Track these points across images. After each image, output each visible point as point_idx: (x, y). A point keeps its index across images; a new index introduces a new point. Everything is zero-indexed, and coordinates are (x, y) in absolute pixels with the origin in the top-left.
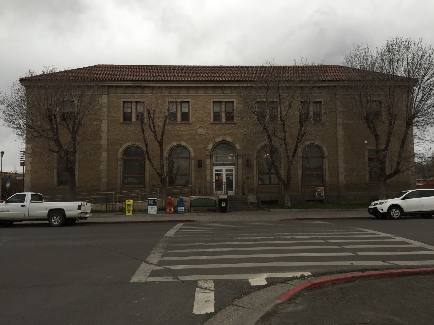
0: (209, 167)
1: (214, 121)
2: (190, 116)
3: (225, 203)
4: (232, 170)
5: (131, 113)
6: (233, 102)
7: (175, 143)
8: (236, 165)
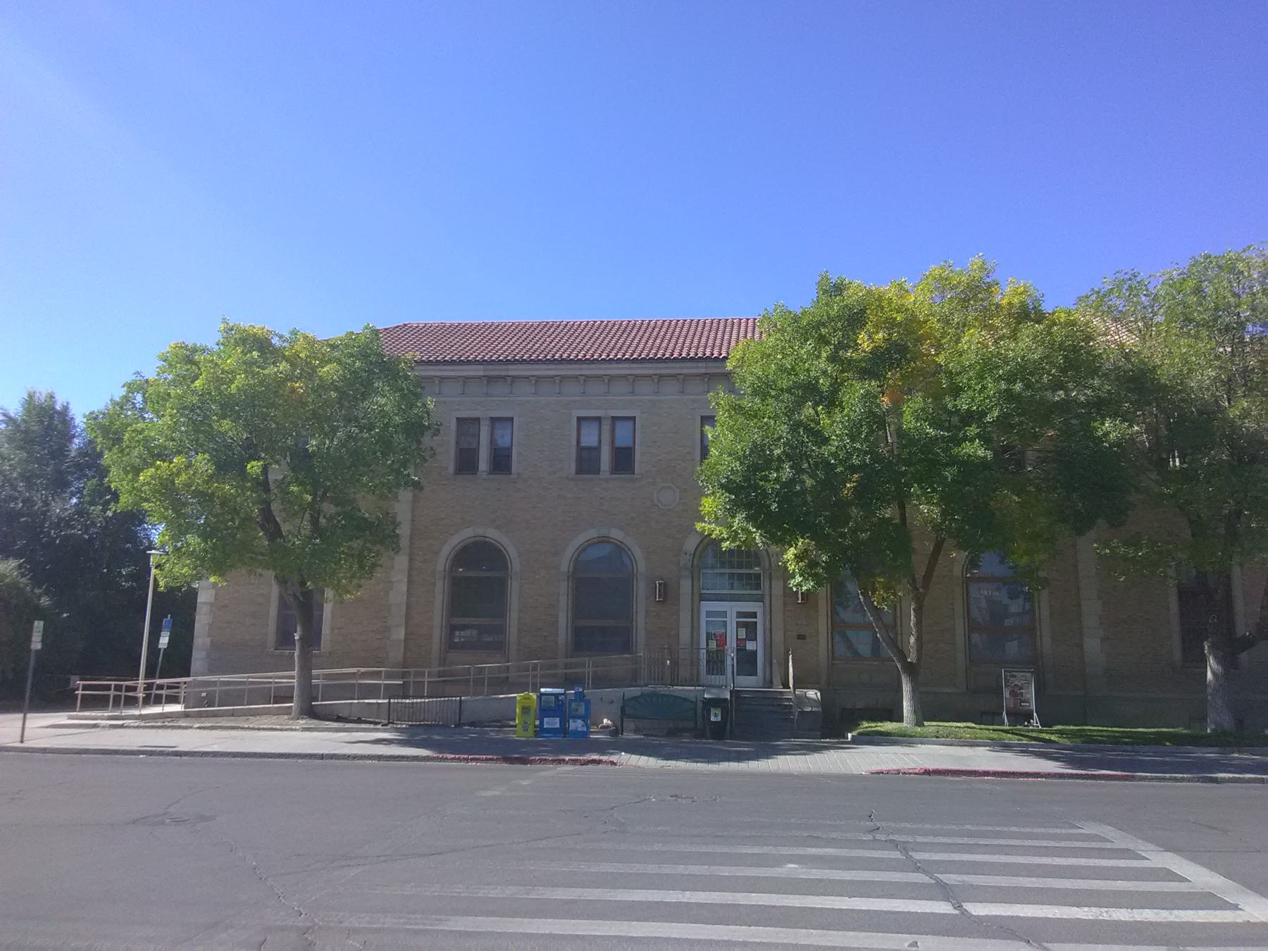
0: (685, 600)
1: (577, 473)
3: (719, 711)
4: (754, 615)
5: (597, 449)
7: (592, 534)
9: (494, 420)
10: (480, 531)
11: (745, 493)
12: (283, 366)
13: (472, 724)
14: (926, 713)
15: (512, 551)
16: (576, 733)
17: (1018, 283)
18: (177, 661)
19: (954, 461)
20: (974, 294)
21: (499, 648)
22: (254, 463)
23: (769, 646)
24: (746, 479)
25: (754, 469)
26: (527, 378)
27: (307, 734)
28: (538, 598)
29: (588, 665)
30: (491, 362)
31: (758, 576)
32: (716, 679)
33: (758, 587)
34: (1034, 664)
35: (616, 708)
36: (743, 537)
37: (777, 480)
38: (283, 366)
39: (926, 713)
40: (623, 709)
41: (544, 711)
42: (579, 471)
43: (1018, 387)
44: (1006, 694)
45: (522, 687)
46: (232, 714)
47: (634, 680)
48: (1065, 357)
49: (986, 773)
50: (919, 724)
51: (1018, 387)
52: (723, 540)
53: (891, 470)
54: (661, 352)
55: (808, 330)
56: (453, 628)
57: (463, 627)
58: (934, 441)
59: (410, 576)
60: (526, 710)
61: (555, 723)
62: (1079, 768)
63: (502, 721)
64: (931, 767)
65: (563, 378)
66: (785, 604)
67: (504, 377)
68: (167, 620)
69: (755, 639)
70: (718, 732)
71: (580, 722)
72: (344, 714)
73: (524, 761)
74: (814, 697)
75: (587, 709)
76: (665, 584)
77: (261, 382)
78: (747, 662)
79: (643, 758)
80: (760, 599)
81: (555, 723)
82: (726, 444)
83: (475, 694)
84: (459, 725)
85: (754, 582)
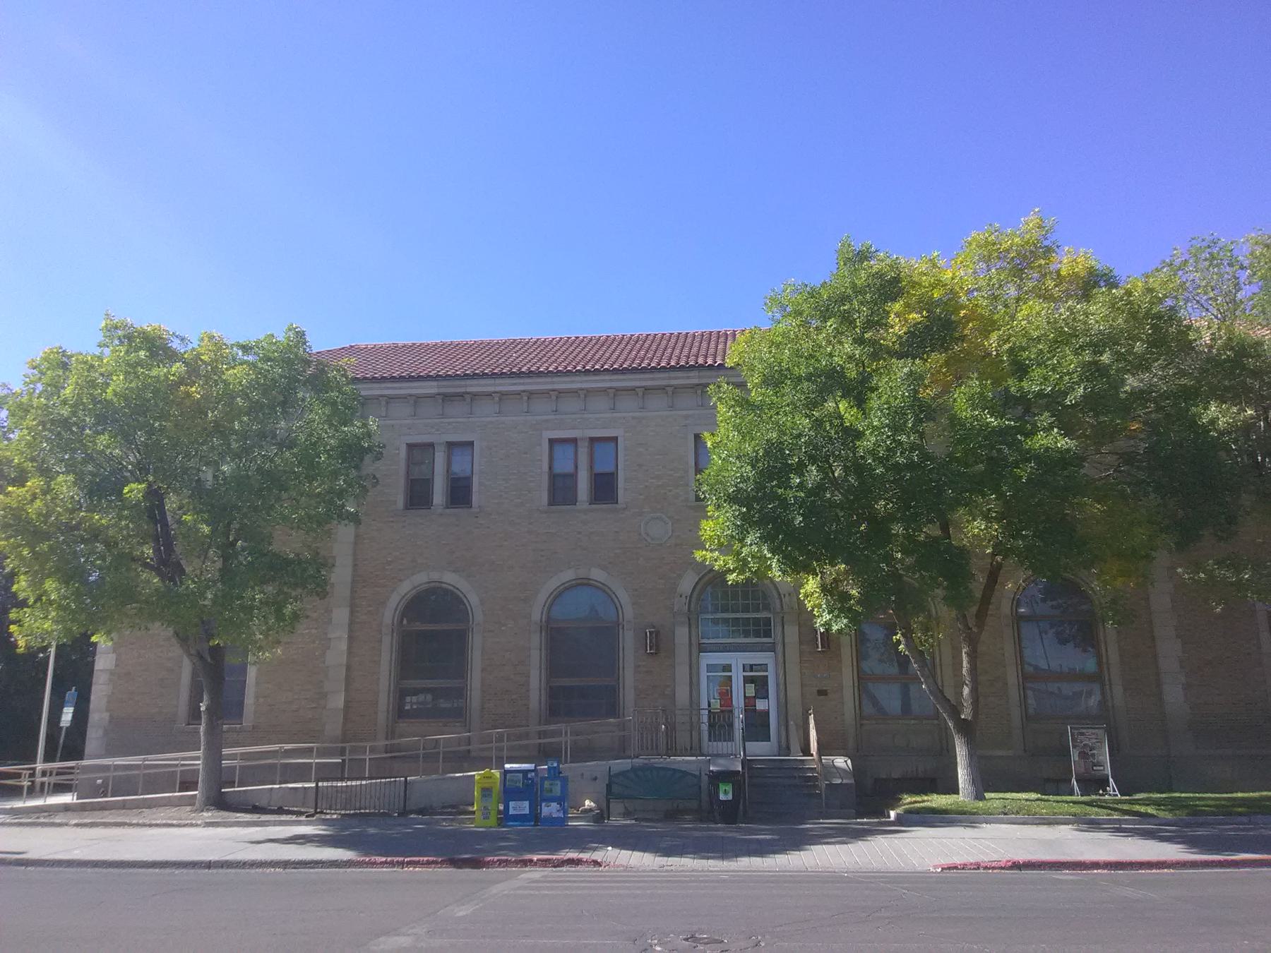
2: (475, 488)
3: (729, 788)
4: (764, 667)
5: (573, 476)
6: (471, 444)
7: (568, 575)
8: (779, 648)
9: (451, 445)
10: (435, 576)
11: (761, 507)
12: (178, 367)
13: (421, 812)
14: (987, 781)
15: (473, 599)
16: (551, 820)
17: (1077, 252)
18: (70, 745)
19: (1027, 456)
20: (1027, 262)
21: (459, 715)
22: (133, 486)
23: (784, 707)
24: (759, 487)
25: (767, 475)
26: (489, 395)
27: (211, 831)
28: (505, 655)
29: (566, 733)
30: (447, 377)
31: (767, 622)
32: (722, 747)
33: (767, 634)
34: (1104, 718)
35: (601, 786)
36: (754, 566)
37: (801, 486)
38: (178, 367)
39: (987, 781)
40: (609, 786)
41: (510, 793)
42: (551, 504)
43: (1106, 358)
44: (1074, 755)
45: (484, 762)
46: (124, 806)
47: (621, 751)
48: (1153, 326)
49: (1096, 865)
50: (979, 797)
51: (1106, 358)
52: (730, 571)
53: (927, 486)
54: (646, 362)
55: (830, 307)
56: (402, 694)
57: (416, 692)
58: (1002, 432)
59: (351, 631)
60: (486, 792)
61: (524, 807)
62: (1218, 852)
63: (458, 808)
64: (1022, 857)
65: (531, 394)
66: (801, 653)
67: (461, 395)
68: (71, 694)
69: (767, 697)
70: (730, 814)
71: (554, 805)
72: (263, 803)
73: (476, 864)
74: (843, 765)
75: (564, 787)
76: (657, 633)
77: (145, 387)
78: (757, 726)
79: (637, 854)
80: (772, 648)
81: (524, 807)
82: (729, 445)
83: (425, 772)
84: (404, 813)
85: (763, 628)
